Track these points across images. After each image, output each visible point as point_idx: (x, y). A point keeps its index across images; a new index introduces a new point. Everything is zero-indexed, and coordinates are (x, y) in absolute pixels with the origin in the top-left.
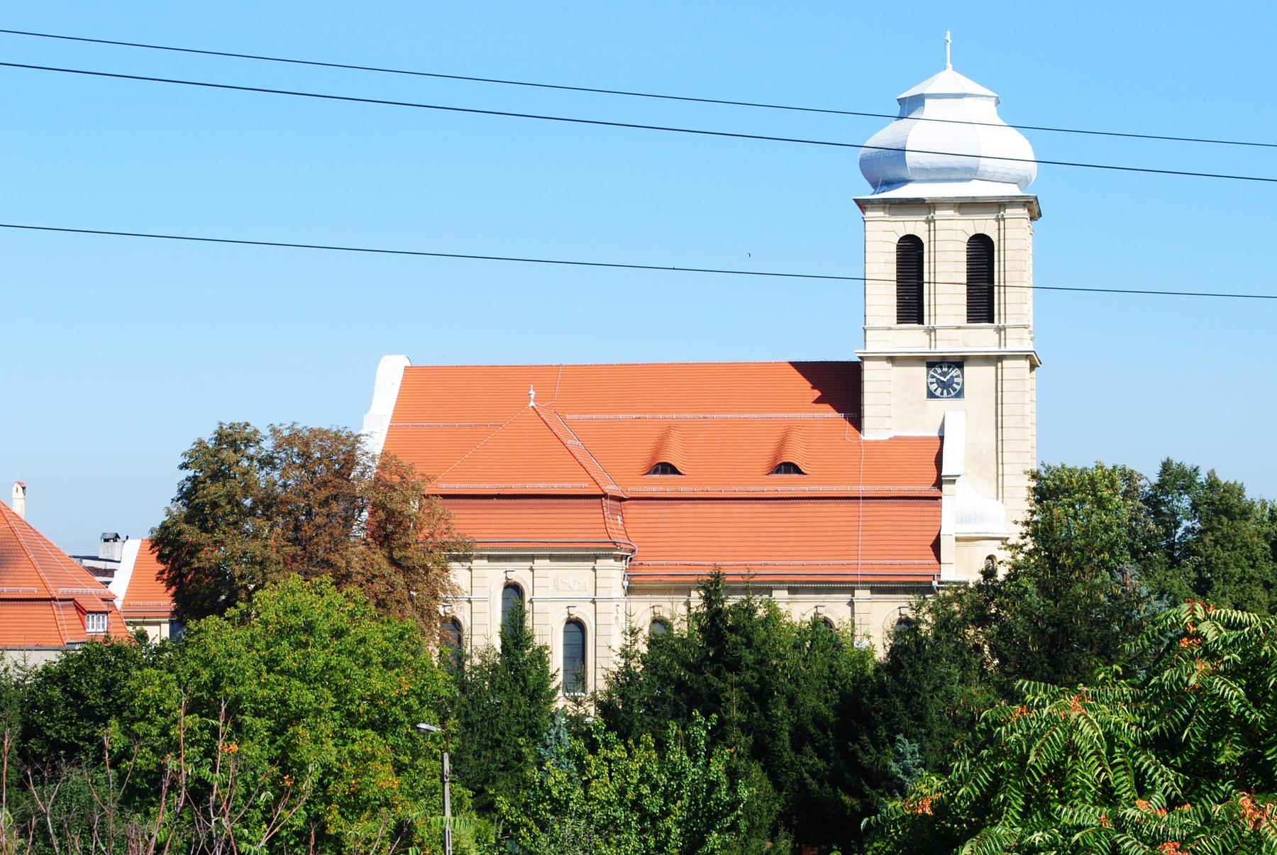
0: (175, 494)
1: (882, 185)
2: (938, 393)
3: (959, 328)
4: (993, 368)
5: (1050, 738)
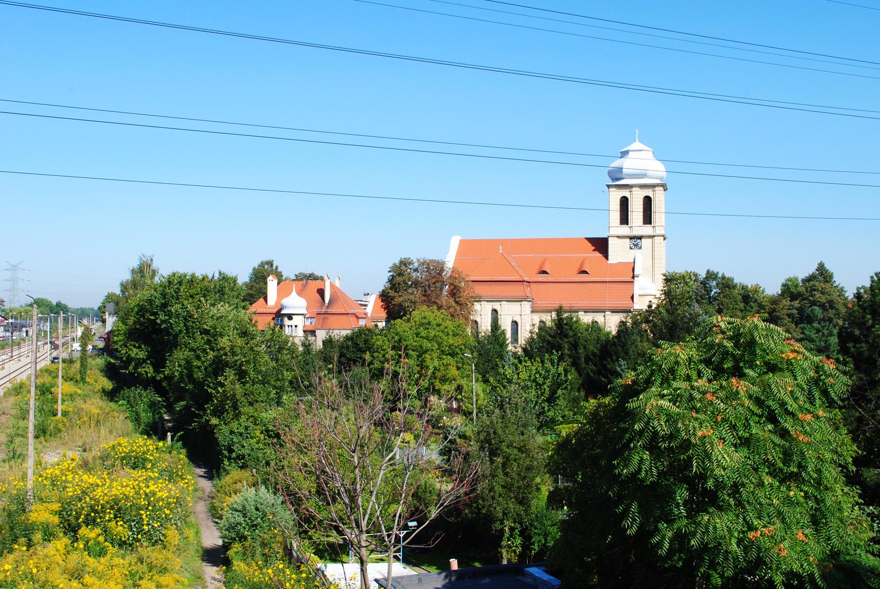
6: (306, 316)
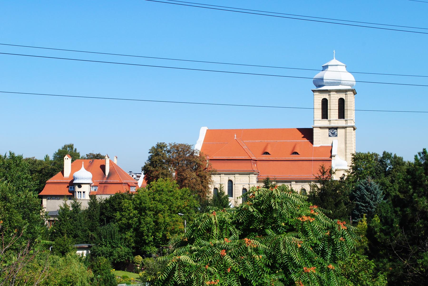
0: (148, 159)
1: (318, 86)
2: (331, 135)
3: (336, 120)
4: (344, 130)
5: (205, 222)
6: (92, 185)
